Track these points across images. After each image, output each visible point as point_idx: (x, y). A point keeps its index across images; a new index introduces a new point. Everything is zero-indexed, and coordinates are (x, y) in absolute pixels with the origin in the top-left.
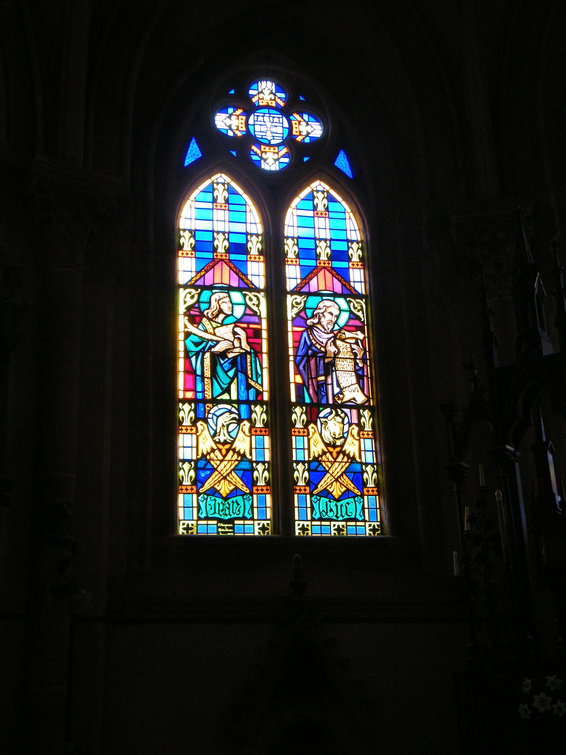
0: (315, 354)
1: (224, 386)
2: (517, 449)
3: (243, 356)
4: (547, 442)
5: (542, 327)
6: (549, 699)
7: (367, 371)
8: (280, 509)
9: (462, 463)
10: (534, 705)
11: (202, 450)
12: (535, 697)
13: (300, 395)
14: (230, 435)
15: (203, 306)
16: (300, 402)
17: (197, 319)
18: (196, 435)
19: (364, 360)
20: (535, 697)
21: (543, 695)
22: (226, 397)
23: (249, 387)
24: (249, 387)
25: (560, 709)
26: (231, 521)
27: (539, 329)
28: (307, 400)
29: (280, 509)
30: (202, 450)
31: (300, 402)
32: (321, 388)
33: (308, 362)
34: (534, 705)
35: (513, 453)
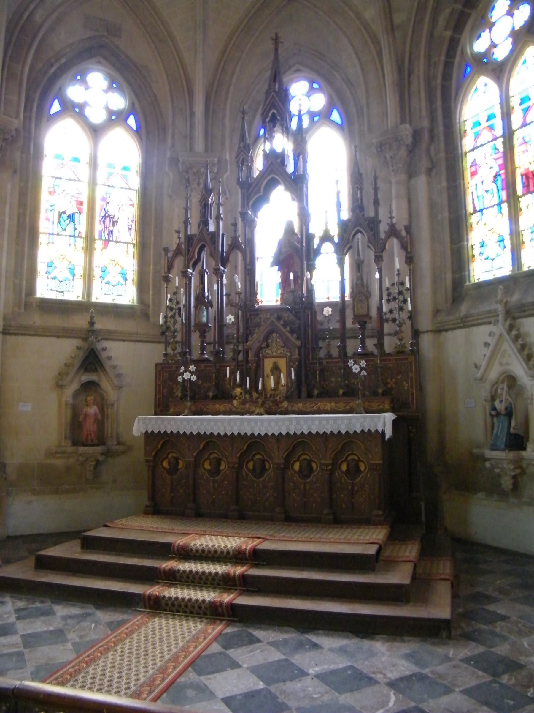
0: (109, 216)
1: (64, 228)
2: (193, 271)
3: (74, 214)
4: (206, 270)
5: (211, 218)
6: (190, 374)
7: (133, 227)
8: (86, 288)
9: (170, 275)
10: (184, 376)
11: (128, 197)
12: (184, 373)
13: (100, 236)
14: (188, 668)
15: (56, 188)
16: (100, 238)
17: (52, 193)
18: (97, 240)
19: (132, 221)
20: (184, 373)
21: (188, 373)
22: (64, 233)
23: (75, 229)
24: (75, 229)
25: (193, 378)
26: (62, 292)
27: (209, 219)
28: (103, 238)
29: (86, 288)
30: (128, 197)
31: (100, 238)
32: (110, 232)
33: (105, 219)
34: (184, 376)
35: (192, 274)
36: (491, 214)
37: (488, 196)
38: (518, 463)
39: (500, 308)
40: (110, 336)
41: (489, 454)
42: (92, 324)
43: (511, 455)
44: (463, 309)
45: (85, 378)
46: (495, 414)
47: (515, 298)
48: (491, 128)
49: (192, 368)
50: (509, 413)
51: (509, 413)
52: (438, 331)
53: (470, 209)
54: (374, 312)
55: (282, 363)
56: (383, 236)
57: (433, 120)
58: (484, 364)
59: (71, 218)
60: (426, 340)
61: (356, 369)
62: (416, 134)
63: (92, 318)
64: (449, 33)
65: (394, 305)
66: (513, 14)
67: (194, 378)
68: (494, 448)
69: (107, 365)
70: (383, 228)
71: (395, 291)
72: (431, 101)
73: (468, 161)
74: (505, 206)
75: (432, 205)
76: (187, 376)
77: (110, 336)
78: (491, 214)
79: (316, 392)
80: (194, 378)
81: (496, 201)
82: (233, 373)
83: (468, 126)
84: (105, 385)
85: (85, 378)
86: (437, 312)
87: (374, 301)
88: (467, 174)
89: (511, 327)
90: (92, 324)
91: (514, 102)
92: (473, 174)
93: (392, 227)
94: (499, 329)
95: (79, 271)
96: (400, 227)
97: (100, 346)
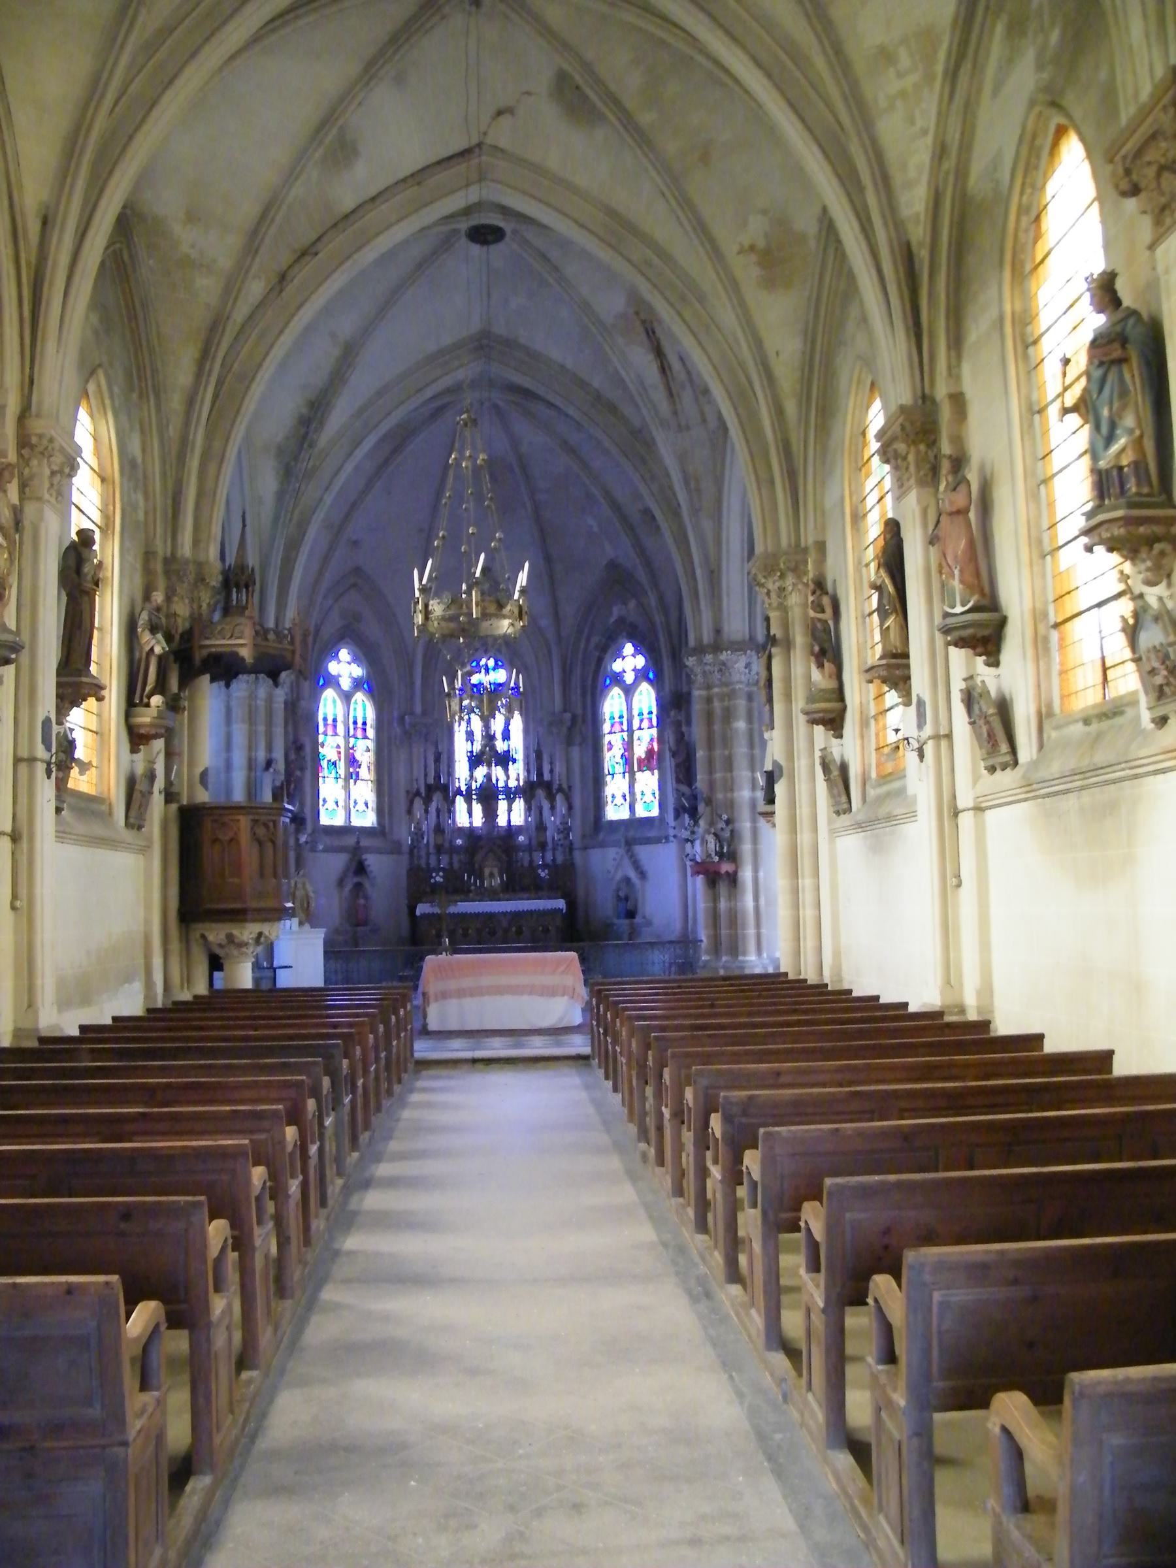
36: (618, 777)
37: (617, 766)
38: (632, 926)
39: (623, 840)
40: (368, 850)
41: (616, 921)
42: (358, 842)
43: (627, 921)
44: (601, 836)
45: (356, 880)
46: (619, 898)
47: (631, 833)
48: (621, 723)
49: (441, 874)
50: (627, 899)
51: (627, 899)
52: (585, 848)
53: (606, 772)
54: (549, 840)
55: (496, 871)
56: (554, 791)
57: (584, 708)
58: (613, 871)
59: (334, 764)
60: (578, 856)
61: (543, 874)
62: (574, 718)
63: (358, 838)
64: (597, 654)
65: (561, 836)
66: (643, 771)
67: (442, 880)
68: (619, 917)
69: (368, 869)
70: (555, 787)
71: (561, 827)
72: (584, 695)
73: (607, 739)
74: (627, 775)
75: (582, 767)
76: (438, 879)
77: (368, 850)
78: (618, 777)
79: (321, 847)
80: (442, 880)
81: (622, 771)
82: (469, 878)
83: (607, 717)
84: (367, 885)
85: (356, 880)
86: (584, 837)
87: (549, 834)
88: (606, 748)
89: (628, 851)
90: (358, 842)
91: (635, 712)
92: (610, 749)
93: (560, 785)
94: (622, 851)
95: (341, 803)
96: (565, 786)
97: (364, 857)
